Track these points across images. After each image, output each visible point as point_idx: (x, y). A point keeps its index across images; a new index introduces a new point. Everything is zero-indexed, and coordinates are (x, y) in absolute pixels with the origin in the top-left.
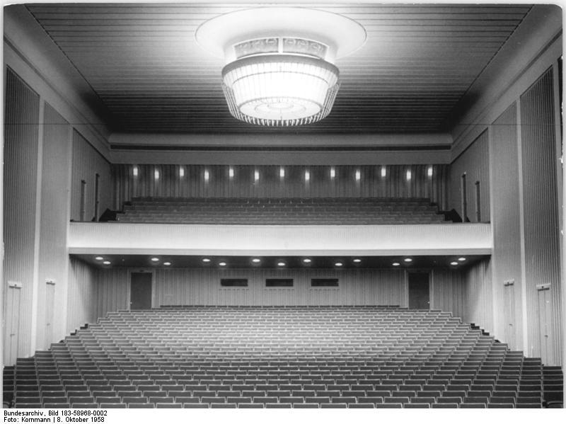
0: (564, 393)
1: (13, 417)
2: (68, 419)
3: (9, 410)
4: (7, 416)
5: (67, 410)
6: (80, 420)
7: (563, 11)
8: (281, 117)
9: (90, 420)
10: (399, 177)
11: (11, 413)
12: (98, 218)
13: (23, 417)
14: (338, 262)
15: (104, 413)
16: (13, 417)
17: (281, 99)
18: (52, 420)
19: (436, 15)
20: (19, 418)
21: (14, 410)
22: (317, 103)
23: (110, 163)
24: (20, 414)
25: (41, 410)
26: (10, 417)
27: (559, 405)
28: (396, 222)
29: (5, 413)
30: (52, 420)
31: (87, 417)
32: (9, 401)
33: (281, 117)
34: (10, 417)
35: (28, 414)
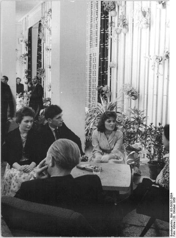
1: (173, 232)
2: (174, 213)
3: (170, 234)
4: (173, 235)
5: (170, 210)
9: (174, 204)
10: (26, 169)
13: (173, 228)
14: (157, 188)
16: (173, 232)
17: (49, 58)
18: (174, 221)
19: (165, 66)
20: (173, 230)
21: (170, 232)
23: (118, 37)
24: (172, 230)
26: (173, 234)
29: (171, 236)
30: (174, 221)
32: (168, 235)
34: (173, 234)
35: (172, 226)
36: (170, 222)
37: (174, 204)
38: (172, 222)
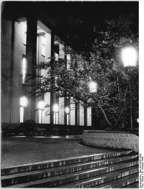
0: (117, 188)
1: (142, 185)
2: (142, 169)
3: (139, 186)
4: (141, 187)
5: (139, 166)
6: (143, 165)
7: (1, 129)
8: (90, 116)
9: (143, 162)
11: (140, 185)
12: (93, 157)
15: (140, 154)
16: (142, 185)
20: (142, 183)
21: (139, 184)
22: (138, 62)
24: (141, 182)
25: (139, 175)
26: (142, 186)
27: (136, 4)
28: (30, 188)
29: (140, 187)
31: (142, 162)
33: (90, 116)
34: (142, 186)
35: (141, 180)
36: (139, 177)
37: (143, 162)
38: (141, 176)
